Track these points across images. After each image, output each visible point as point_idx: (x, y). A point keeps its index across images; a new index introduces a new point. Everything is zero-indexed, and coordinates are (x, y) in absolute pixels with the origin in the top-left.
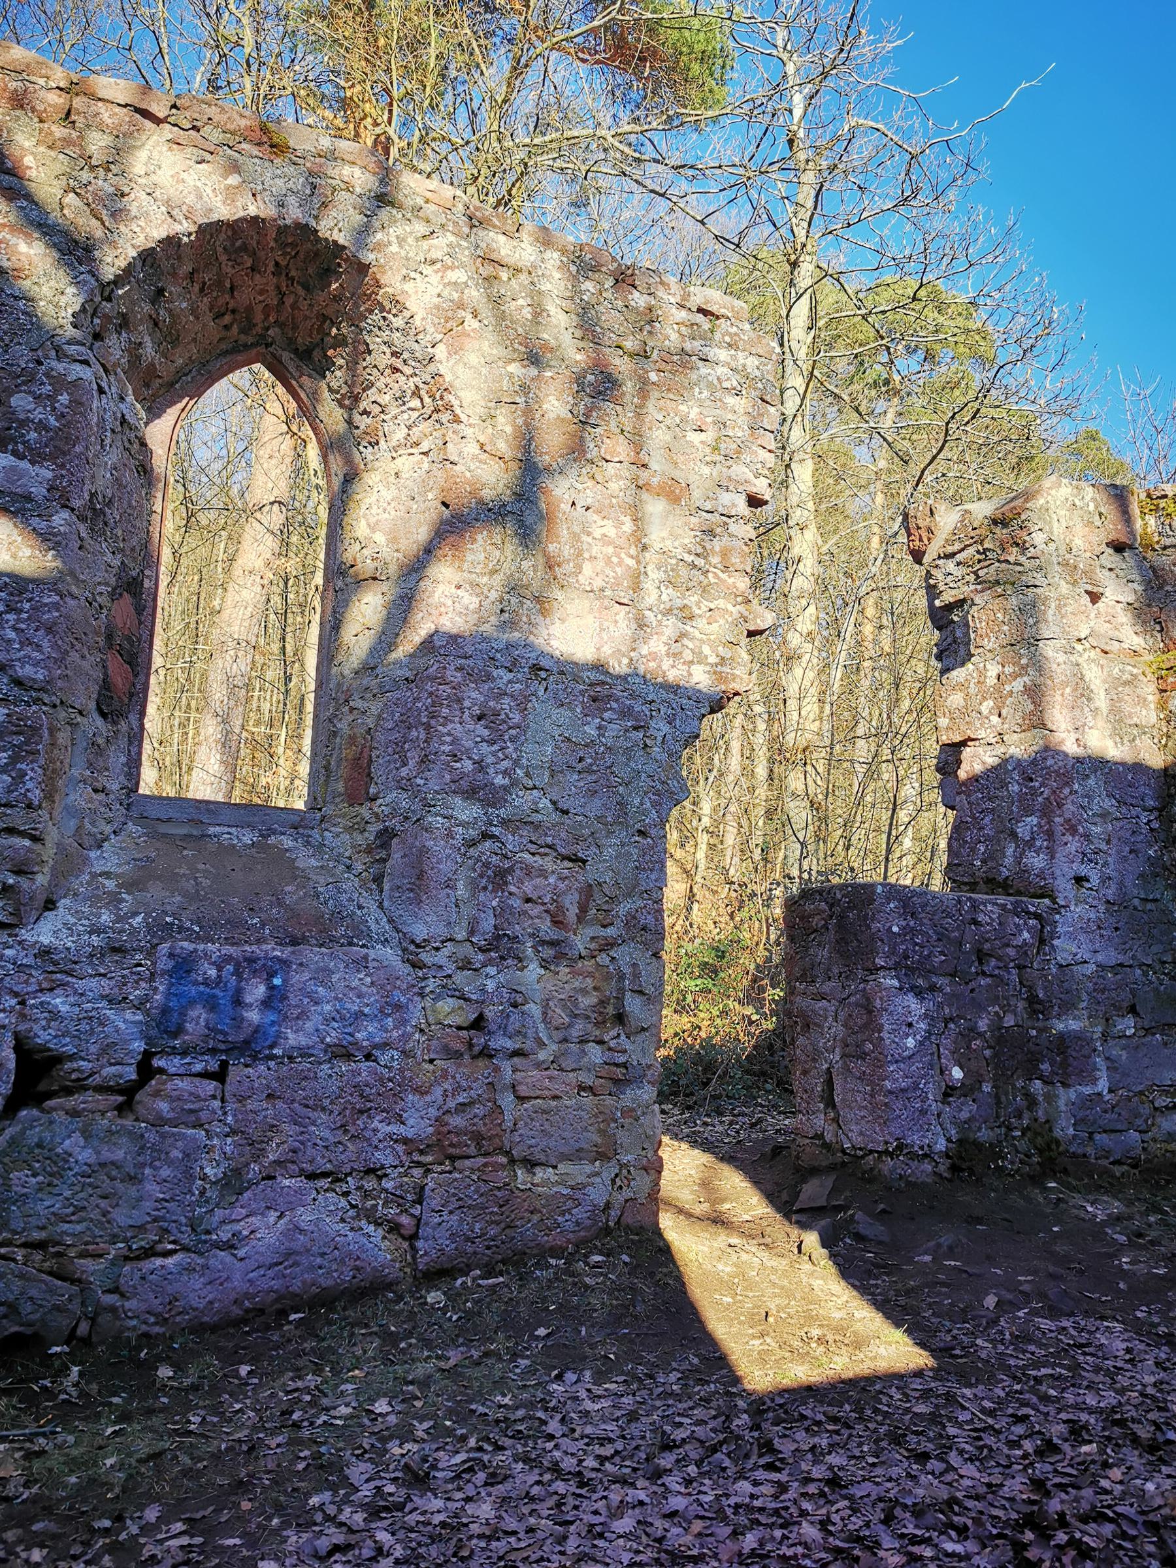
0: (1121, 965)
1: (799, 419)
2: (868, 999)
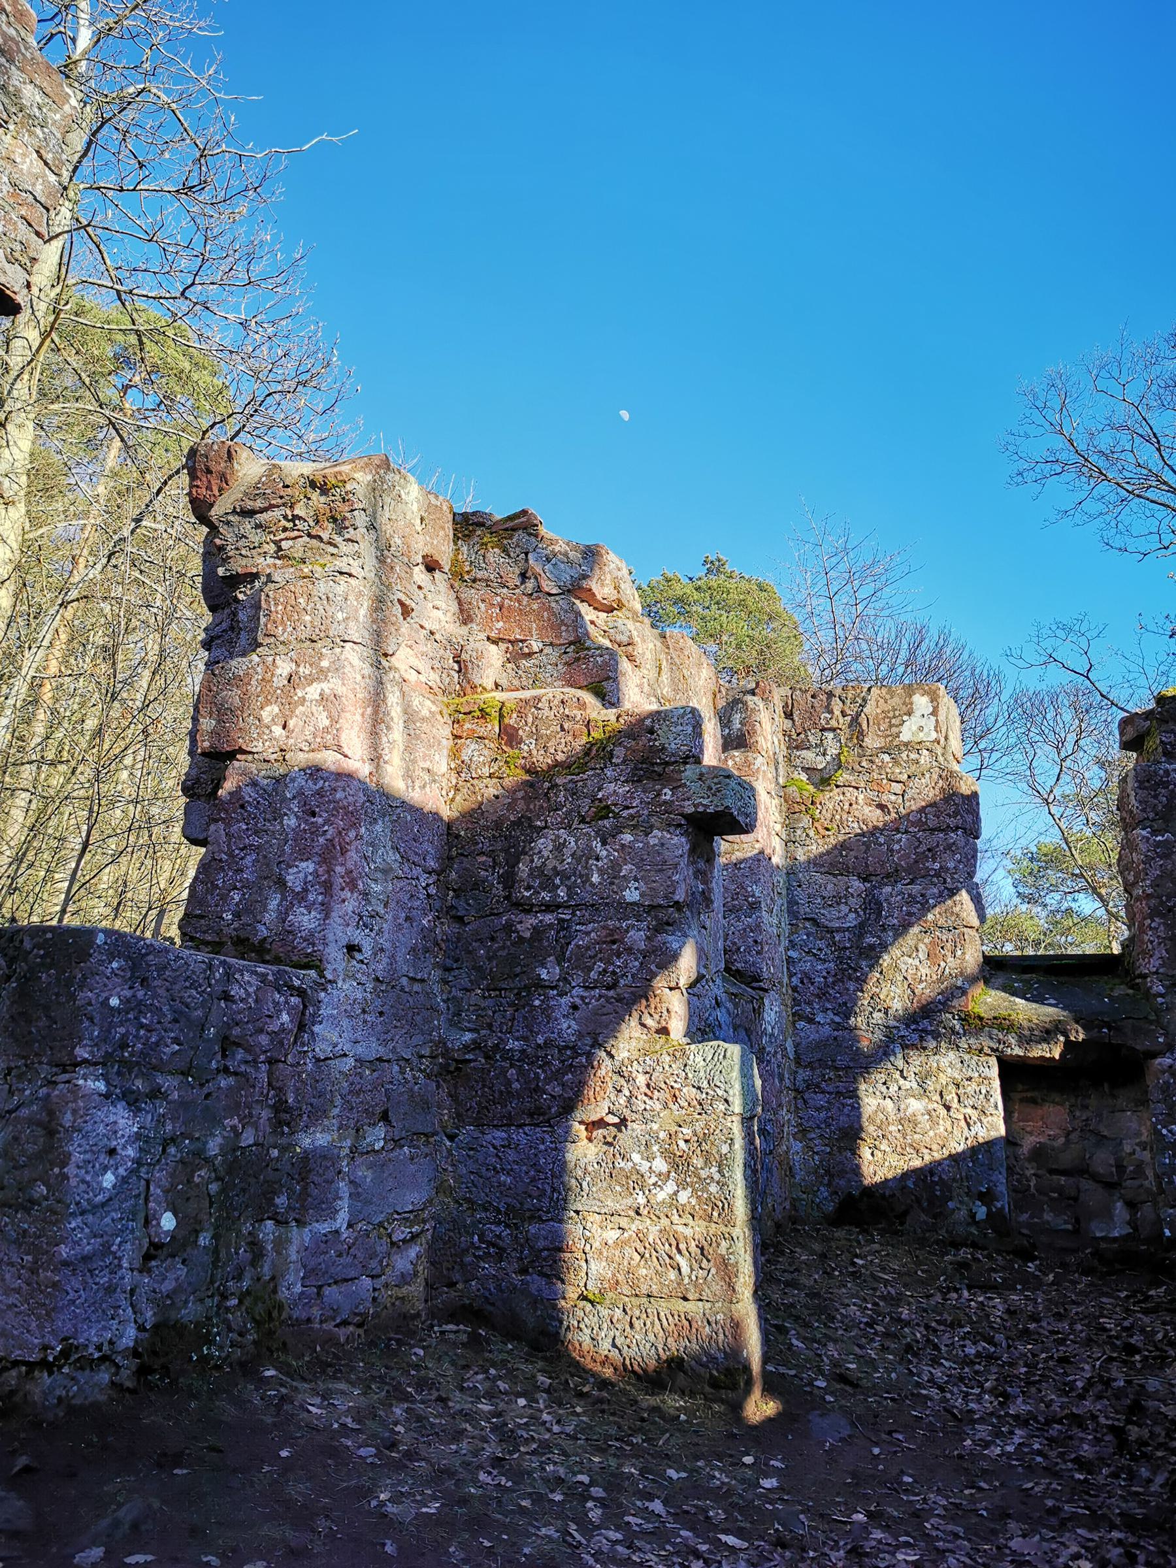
0: (380, 1060)
1: (26, 376)
2: (51, 1113)
